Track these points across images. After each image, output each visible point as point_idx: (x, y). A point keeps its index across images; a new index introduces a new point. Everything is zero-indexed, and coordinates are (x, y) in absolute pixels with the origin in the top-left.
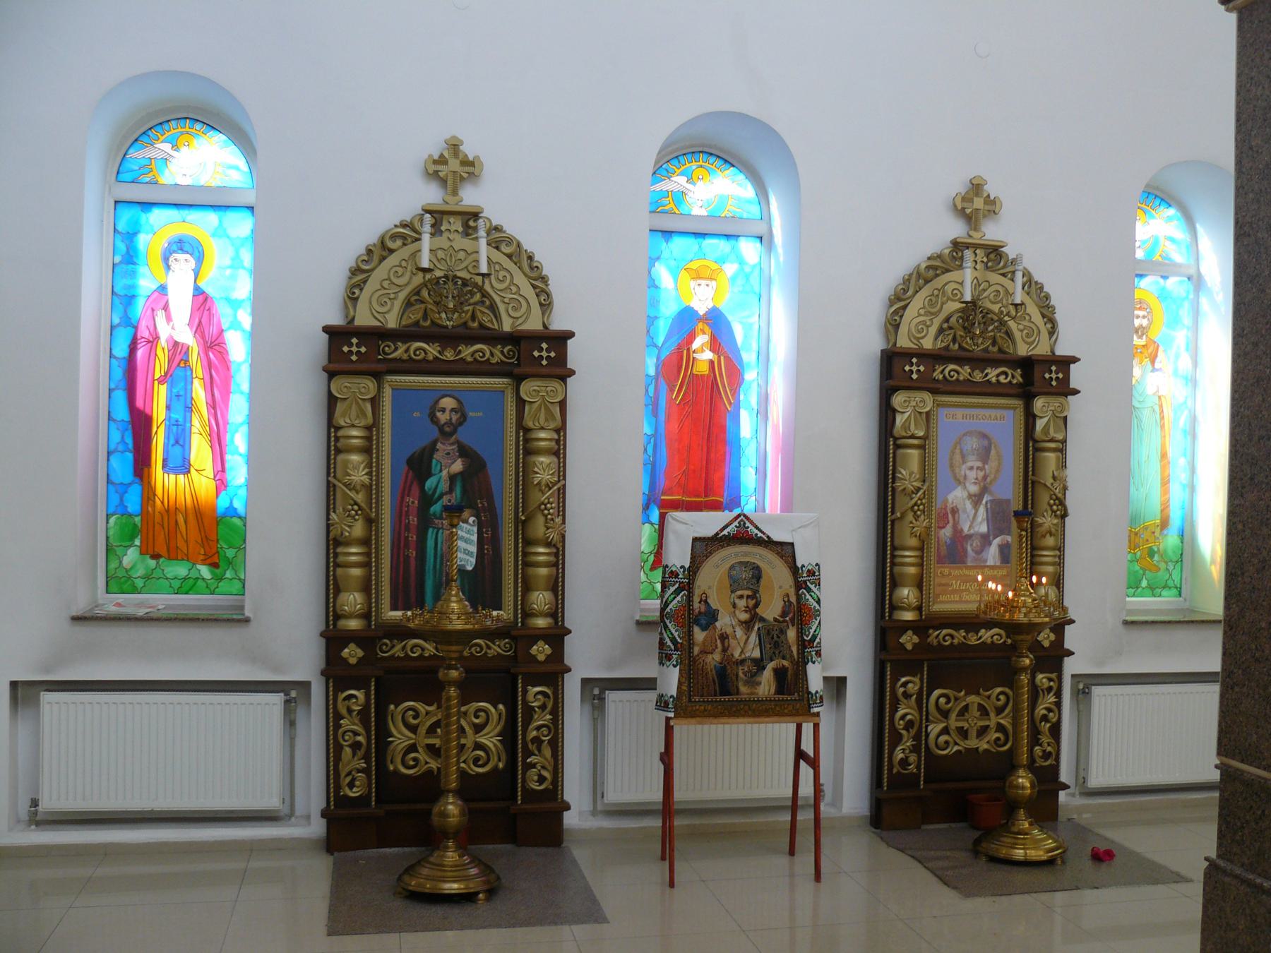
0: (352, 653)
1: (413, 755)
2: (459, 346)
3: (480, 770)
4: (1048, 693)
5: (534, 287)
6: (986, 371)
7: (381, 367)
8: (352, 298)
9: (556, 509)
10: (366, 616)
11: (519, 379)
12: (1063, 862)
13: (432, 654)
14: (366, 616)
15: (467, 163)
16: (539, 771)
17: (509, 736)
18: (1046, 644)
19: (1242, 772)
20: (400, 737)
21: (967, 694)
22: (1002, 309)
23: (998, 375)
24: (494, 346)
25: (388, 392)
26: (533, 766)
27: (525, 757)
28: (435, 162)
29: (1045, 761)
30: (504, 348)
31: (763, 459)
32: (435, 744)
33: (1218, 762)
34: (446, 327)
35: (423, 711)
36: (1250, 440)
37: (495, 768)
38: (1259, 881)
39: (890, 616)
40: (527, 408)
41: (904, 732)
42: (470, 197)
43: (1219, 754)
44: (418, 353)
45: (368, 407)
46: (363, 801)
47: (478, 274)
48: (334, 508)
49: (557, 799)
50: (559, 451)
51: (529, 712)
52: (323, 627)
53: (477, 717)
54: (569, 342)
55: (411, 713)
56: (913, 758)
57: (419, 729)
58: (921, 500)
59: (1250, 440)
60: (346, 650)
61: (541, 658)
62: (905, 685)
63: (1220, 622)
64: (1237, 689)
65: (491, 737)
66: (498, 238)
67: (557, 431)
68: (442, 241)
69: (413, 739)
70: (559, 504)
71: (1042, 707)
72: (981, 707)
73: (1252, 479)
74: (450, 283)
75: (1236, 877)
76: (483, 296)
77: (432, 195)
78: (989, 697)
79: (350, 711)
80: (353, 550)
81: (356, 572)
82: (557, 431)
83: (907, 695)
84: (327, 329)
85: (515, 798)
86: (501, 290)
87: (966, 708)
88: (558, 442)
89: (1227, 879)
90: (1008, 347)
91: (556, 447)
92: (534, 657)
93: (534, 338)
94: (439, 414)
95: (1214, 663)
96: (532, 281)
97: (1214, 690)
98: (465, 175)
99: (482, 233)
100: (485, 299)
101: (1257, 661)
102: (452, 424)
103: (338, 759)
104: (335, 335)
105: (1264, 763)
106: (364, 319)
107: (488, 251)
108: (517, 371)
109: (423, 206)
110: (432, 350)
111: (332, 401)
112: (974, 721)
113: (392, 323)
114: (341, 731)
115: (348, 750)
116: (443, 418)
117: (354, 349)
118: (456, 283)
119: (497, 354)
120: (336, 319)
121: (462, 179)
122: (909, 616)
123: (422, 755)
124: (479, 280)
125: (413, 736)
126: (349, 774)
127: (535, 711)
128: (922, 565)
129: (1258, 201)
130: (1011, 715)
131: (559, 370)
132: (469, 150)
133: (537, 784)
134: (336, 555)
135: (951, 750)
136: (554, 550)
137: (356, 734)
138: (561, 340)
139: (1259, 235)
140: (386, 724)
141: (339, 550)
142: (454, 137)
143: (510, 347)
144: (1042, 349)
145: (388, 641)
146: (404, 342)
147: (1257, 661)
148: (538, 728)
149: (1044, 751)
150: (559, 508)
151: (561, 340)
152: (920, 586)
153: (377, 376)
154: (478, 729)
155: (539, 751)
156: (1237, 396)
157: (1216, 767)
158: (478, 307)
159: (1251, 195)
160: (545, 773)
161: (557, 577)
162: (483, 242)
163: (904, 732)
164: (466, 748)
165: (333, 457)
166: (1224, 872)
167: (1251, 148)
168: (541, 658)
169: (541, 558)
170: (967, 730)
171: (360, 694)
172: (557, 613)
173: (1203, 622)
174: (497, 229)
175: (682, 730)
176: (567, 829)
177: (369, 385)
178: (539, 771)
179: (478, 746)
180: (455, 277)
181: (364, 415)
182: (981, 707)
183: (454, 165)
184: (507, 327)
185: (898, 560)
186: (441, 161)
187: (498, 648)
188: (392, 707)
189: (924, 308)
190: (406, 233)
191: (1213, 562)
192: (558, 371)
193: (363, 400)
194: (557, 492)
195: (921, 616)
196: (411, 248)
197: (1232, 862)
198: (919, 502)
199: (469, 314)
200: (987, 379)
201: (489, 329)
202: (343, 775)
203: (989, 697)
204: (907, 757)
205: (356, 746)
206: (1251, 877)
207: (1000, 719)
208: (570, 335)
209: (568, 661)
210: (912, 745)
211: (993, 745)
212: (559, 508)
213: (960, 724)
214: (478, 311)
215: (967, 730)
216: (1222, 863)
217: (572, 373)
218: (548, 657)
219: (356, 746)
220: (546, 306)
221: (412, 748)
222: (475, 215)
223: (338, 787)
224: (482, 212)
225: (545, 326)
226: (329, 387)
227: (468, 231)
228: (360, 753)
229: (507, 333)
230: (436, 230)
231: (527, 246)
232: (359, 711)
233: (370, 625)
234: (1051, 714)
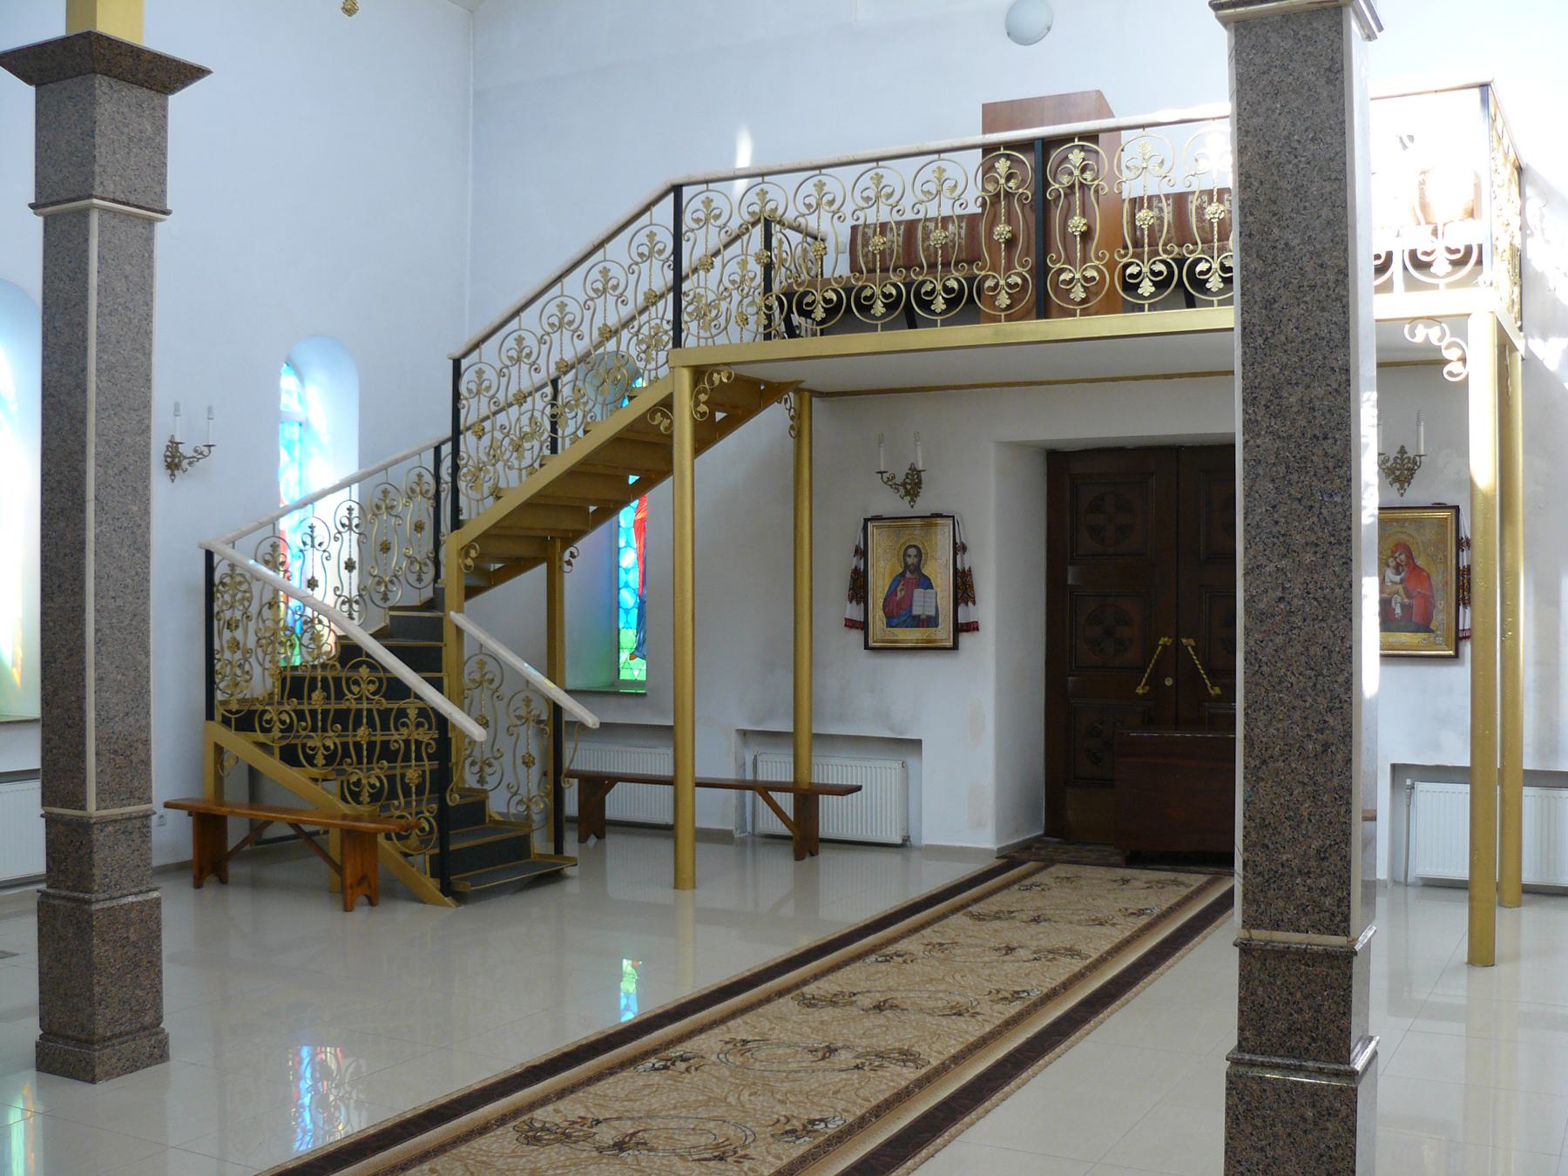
12: (851, 624)
19: (62, 815)
22: (633, 267)
33: (43, 812)
36: (57, 557)
38: (81, 895)
43: (43, 805)
59: (57, 557)
63: (34, 721)
64: (55, 751)
73: (59, 586)
75: (64, 898)
89: (57, 902)
95: (33, 761)
97: (34, 788)
101: (70, 727)
105: (51, 412)
129: (61, 371)
130: (672, 258)
139: (62, 397)
147: (70, 727)
156: (45, 522)
157: (42, 816)
159: (55, 366)
166: (54, 897)
167: (55, 328)
173: (8, 723)
191: (14, 665)
197: (59, 888)
206: (76, 894)
216: (51, 891)
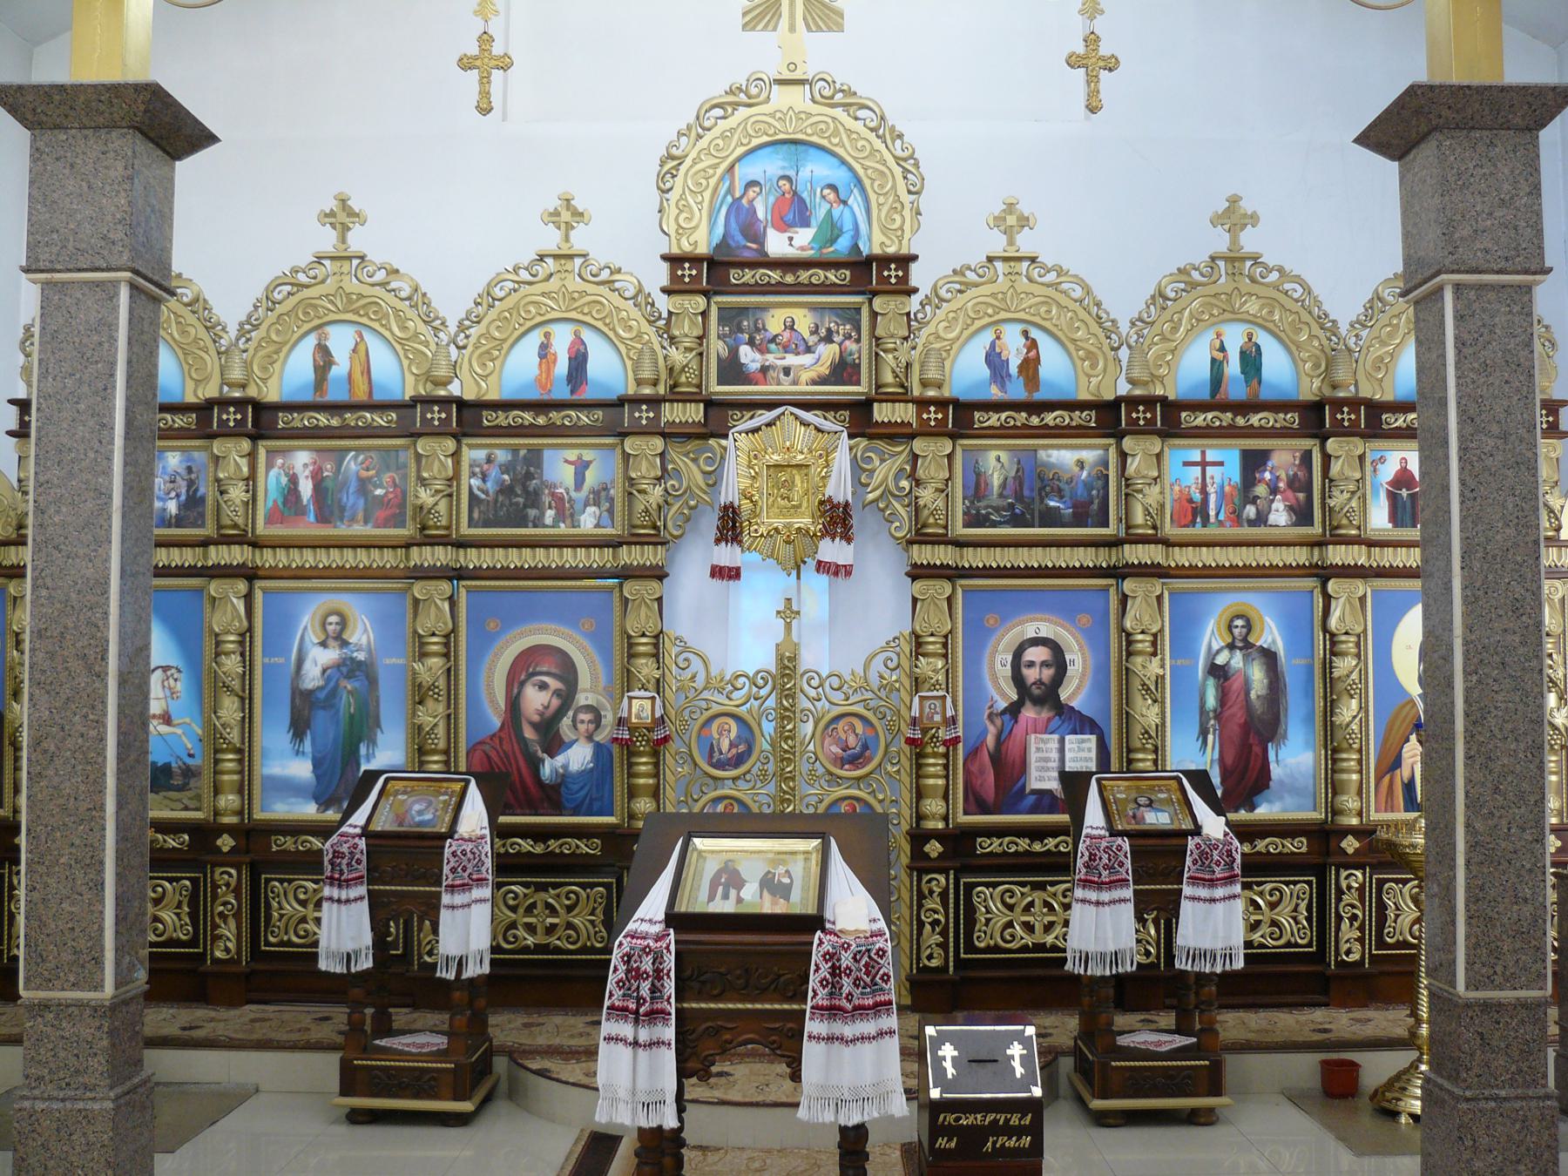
10: (946, 818)
14: (946, 818)
18: (219, 842)
31: (1406, 716)
35: (521, 895)
53: (568, 899)
62: (929, 881)
72: (548, 906)
80: (436, 758)
87: (533, 905)
94: (1025, 671)
102: (1042, 683)
114: (1343, 904)
115: (928, 927)
116: (1031, 675)
122: (1355, 821)
123: (521, 932)
126: (1347, 941)
128: (215, 773)
137: (935, 912)
152: (240, 792)
169: (643, 768)
175: (811, 910)
182: (1047, 904)
202: (923, 948)
213: (1037, 902)
223: (919, 959)
228: (1356, 924)
233: (243, 820)
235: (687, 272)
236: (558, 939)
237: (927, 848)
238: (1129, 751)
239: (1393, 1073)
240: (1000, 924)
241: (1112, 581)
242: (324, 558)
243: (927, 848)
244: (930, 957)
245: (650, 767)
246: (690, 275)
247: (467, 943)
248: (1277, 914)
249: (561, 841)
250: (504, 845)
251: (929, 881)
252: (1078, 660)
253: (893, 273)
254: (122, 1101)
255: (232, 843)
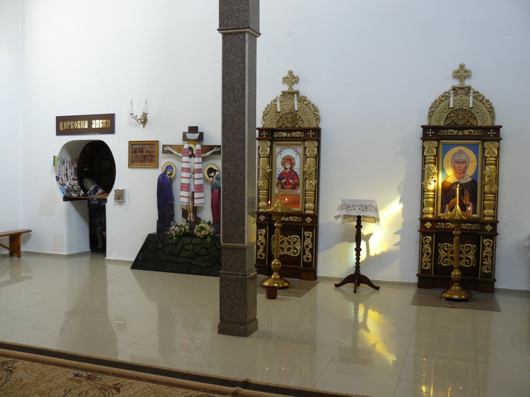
0: (428, 225)
1: (446, 259)
2: (463, 131)
3: (467, 266)
4: (309, 238)
5: (489, 111)
6: (464, 131)
7: (439, 138)
8: (430, 116)
9: (495, 183)
11: (484, 141)
13: (474, 229)
15: (466, 71)
16: (487, 266)
17: (477, 255)
20: (442, 253)
21: (284, 237)
23: (444, 132)
24: (475, 130)
25: (441, 145)
26: (485, 265)
27: (482, 262)
28: (456, 72)
29: (307, 260)
30: (478, 131)
32: (283, 247)
34: (459, 125)
37: (472, 266)
39: (483, 219)
40: (486, 150)
41: (261, 246)
42: (467, 83)
44: (451, 133)
45: (435, 150)
46: (429, 271)
47: (469, 108)
48: (424, 180)
49: (492, 278)
50: (497, 164)
51: (484, 247)
52: (420, 217)
54: (501, 129)
55: (446, 246)
56: (263, 255)
57: (293, 244)
58: (311, 173)
60: (487, 227)
61: (489, 230)
62: (260, 231)
65: (471, 255)
66: (477, 96)
67: (496, 157)
68: (458, 97)
69: (446, 254)
70: (496, 180)
71: (306, 243)
72: (288, 241)
74: (461, 111)
76: (472, 115)
77: (456, 83)
78: (463, 247)
79: (426, 243)
81: (431, 200)
82: (435, 156)
83: (261, 235)
84: (422, 126)
85: (300, 265)
86: (314, 111)
87: (283, 241)
88: (496, 161)
90: (474, 122)
91: (496, 163)
92: (306, 221)
93: (487, 129)
96: (488, 109)
98: (466, 76)
99: (471, 94)
100: (472, 116)
103: (422, 258)
104: (425, 128)
106: (434, 123)
107: (473, 100)
108: (483, 138)
109: (452, 86)
110: (455, 132)
111: (424, 148)
112: (285, 246)
113: (442, 124)
117: (491, 133)
118: (463, 111)
119: (476, 133)
120: (426, 123)
121: (465, 77)
122: (431, 216)
124: (470, 109)
125: (446, 254)
127: (486, 247)
131: (497, 138)
132: (467, 67)
133: (486, 271)
134: (484, 197)
135: (449, 264)
136: (495, 196)
137: (428, 250)
138: (497, 129)
140: (438, 249)
141: (486, 195)
142: (462, 64)
143: (481, 130)
144: (488, 124)
145: (440, 224)
146: (446, 130)
148: (487, 253)
149: (307, 257)
150: (496, 182)
151: (497, 129)
153: (438, 141)
154: (467, 252)
155: (487, 260)
158: (470, 118)
160: (488, 267)
161: (495, 205)
162: (471, 98)
163: (261, 246)
164: (463, 258)
165: (484, 166)
168: (489, 230)
170: (284, 248)
171: (430, 238)
172: (495, 216)
174: (477, 92)
176: (319, 276)
177: (435, 143)
178: (487, 266)
179: (467, 258)
180: (463, 109)
181: (433, 152)
182: (288, 241)
183: (462, 73)
184: (480, 124)
185: (314, 192)
186: (458, 72)
187: (296, 219)
188: (440, 244)
189: (441, 110)
190: (445, 96)
192: (497, 138)
193: (434, 148)
194: (315, 171)
195: (434, 216)
196: (447, 101)
198: (310, 174)
199: (467, 120)
200: (464, 134)
201: (473, 125)
203: (463, 247)
204: (261, 254)
205: (428, 254)
207: (467, 255)
208: (501, 127)
209: (498, 232)
210: (263, 251)
211: (465, 264)
212: (496, 182)
214: (470, 120)
215: (284, 248)
217: (501, 139)
218: (491, 230)
219: (428, 254)
220: (493, 117)
221: (446, 257)
222: (469, 88)
223: (422, 266)
224: (471, 87)
225: (492, 124)
226: (423, 144)
227: (467, 94)
229: (479, 126)
230: (456, 94)
231: (487, 97)
232: (429, 243)
234: (310, 245)
235: (311, 134)
236: (462, 263)
237: (306, 219)
238: (306, 191)
239: (358, 395)
240: (442, 257)
241: (480, 141)
242: (135, 143)
243: (306, 219)
244: (426, 266)
245: (266, 196)
246: (310, 135)
247: (87, 252)
248: (445, 254)
249: (294, 217)
250: (444, 226)
251: (426, 239)
252: (298, 161)
253: (311, 134)
254: (114, 386)
255: (264, 218)
